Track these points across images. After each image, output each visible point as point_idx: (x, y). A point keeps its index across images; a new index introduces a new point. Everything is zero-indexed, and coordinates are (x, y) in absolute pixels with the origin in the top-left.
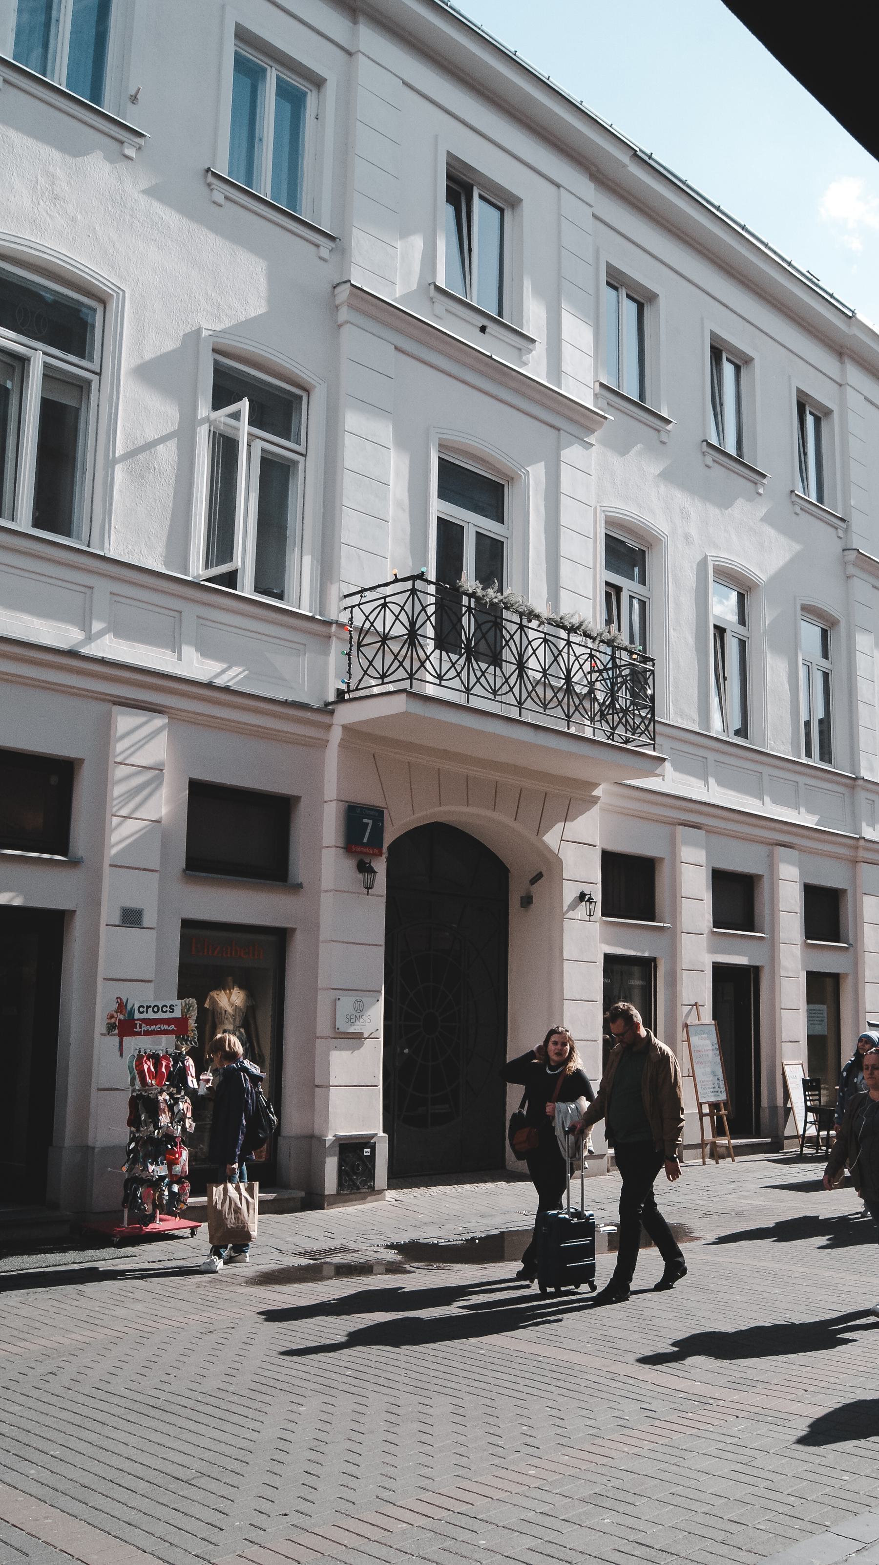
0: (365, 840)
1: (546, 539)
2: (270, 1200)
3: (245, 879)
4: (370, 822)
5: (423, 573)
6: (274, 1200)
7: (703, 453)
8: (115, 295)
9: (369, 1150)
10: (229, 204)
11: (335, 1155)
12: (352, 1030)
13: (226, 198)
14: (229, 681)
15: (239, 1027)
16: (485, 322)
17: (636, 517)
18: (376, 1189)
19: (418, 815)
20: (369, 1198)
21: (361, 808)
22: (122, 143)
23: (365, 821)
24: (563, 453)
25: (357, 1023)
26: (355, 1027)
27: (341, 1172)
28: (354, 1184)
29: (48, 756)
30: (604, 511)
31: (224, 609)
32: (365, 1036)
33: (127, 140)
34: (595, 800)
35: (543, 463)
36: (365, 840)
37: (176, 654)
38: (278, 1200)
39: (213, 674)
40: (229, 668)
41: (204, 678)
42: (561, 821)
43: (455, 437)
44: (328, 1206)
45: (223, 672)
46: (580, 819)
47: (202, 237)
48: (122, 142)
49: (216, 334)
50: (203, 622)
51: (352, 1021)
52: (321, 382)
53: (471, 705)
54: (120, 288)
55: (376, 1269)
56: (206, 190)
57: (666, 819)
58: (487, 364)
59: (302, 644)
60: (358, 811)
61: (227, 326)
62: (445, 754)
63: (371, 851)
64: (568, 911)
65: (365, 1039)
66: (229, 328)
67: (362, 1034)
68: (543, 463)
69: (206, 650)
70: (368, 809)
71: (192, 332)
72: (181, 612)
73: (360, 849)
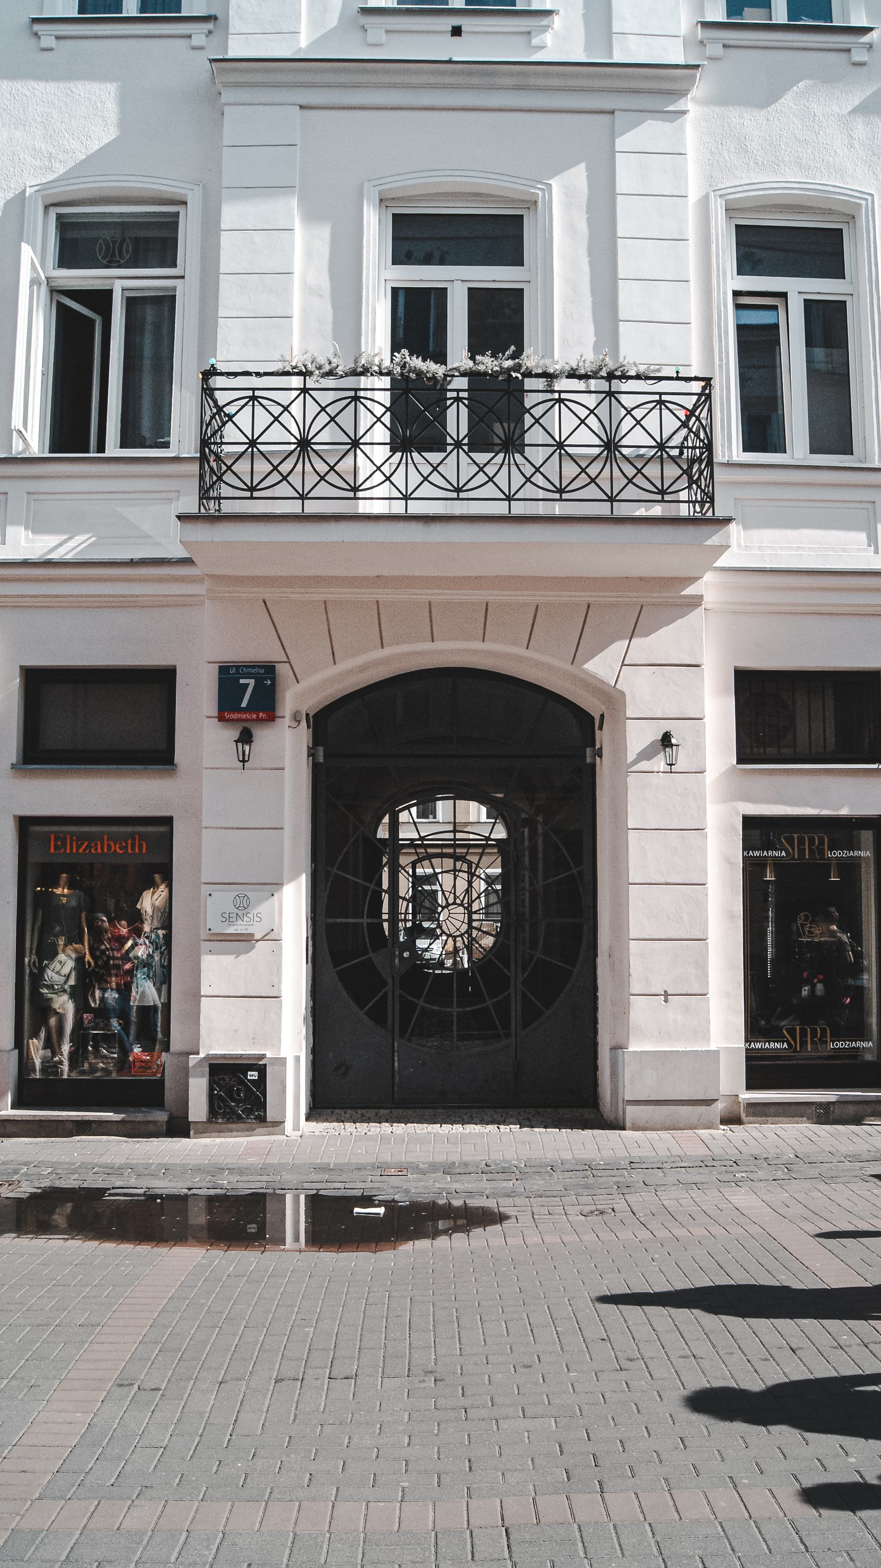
0: (244, 704)
1: (591, 264)
2: (116, 1121)
3: (101, 767)
4: (252, 682)
5: (213, 365)
6: (122, 1122)
7: (702, 42)
8: (863, 202)
9: (256, 1073)
10: (63, 43)
11: (202, 1076)
12: (231, 930)
13: (58, 38)
14: (65, 554)
15: (157, 929)
16: (456, 21)
17: (796, 186)
18: (268, 1120)
19: (344, 665)
20: (258, 1130)
21: (237, 667)
22: (190, 37)
23: (242, 681)
24: (618, 141)
25: (240, 922)
26: (236, 927)
27: (212, 1098)
28: (233, 1112)
29: (121, 668)
30: (721, 196)
31: (50, 477)
32: (257, 937)
33: (195, 31)
34: (696, 602)
35: (582, 166)
36: (244, 704)
37: (873, 547)
38: (126, 1121)
39: (46, 550)
40: (70, 538)
41: (33, 555)
42: (622, 638)
43: (395, 184)
44: (195, 1134)
45: (61, 545)
46: (664, 632)
47: (27, 93)
48: (190, 37)
49: (44, 187)
50: (35, 497)
51: (231, 920)
52: (194, 187)
53: (514, 512)
54: (866, 193)
55: (198, 1217)
56: (33, 40)
57: (875, 609)
58: (453, 73)
59: (175, 491)
60: (233, 671)
61: (61, 173)
62: (379, 581)
63: (254, 716)
64: (636, 762)
65: (257, 941)
66: (64, 174)
67: (252, 935)
68: (582, 166)
69: (37, 527)
70: (247, 667)
71: (19, 193)
72: (6, 493)
73: (235, 716)
